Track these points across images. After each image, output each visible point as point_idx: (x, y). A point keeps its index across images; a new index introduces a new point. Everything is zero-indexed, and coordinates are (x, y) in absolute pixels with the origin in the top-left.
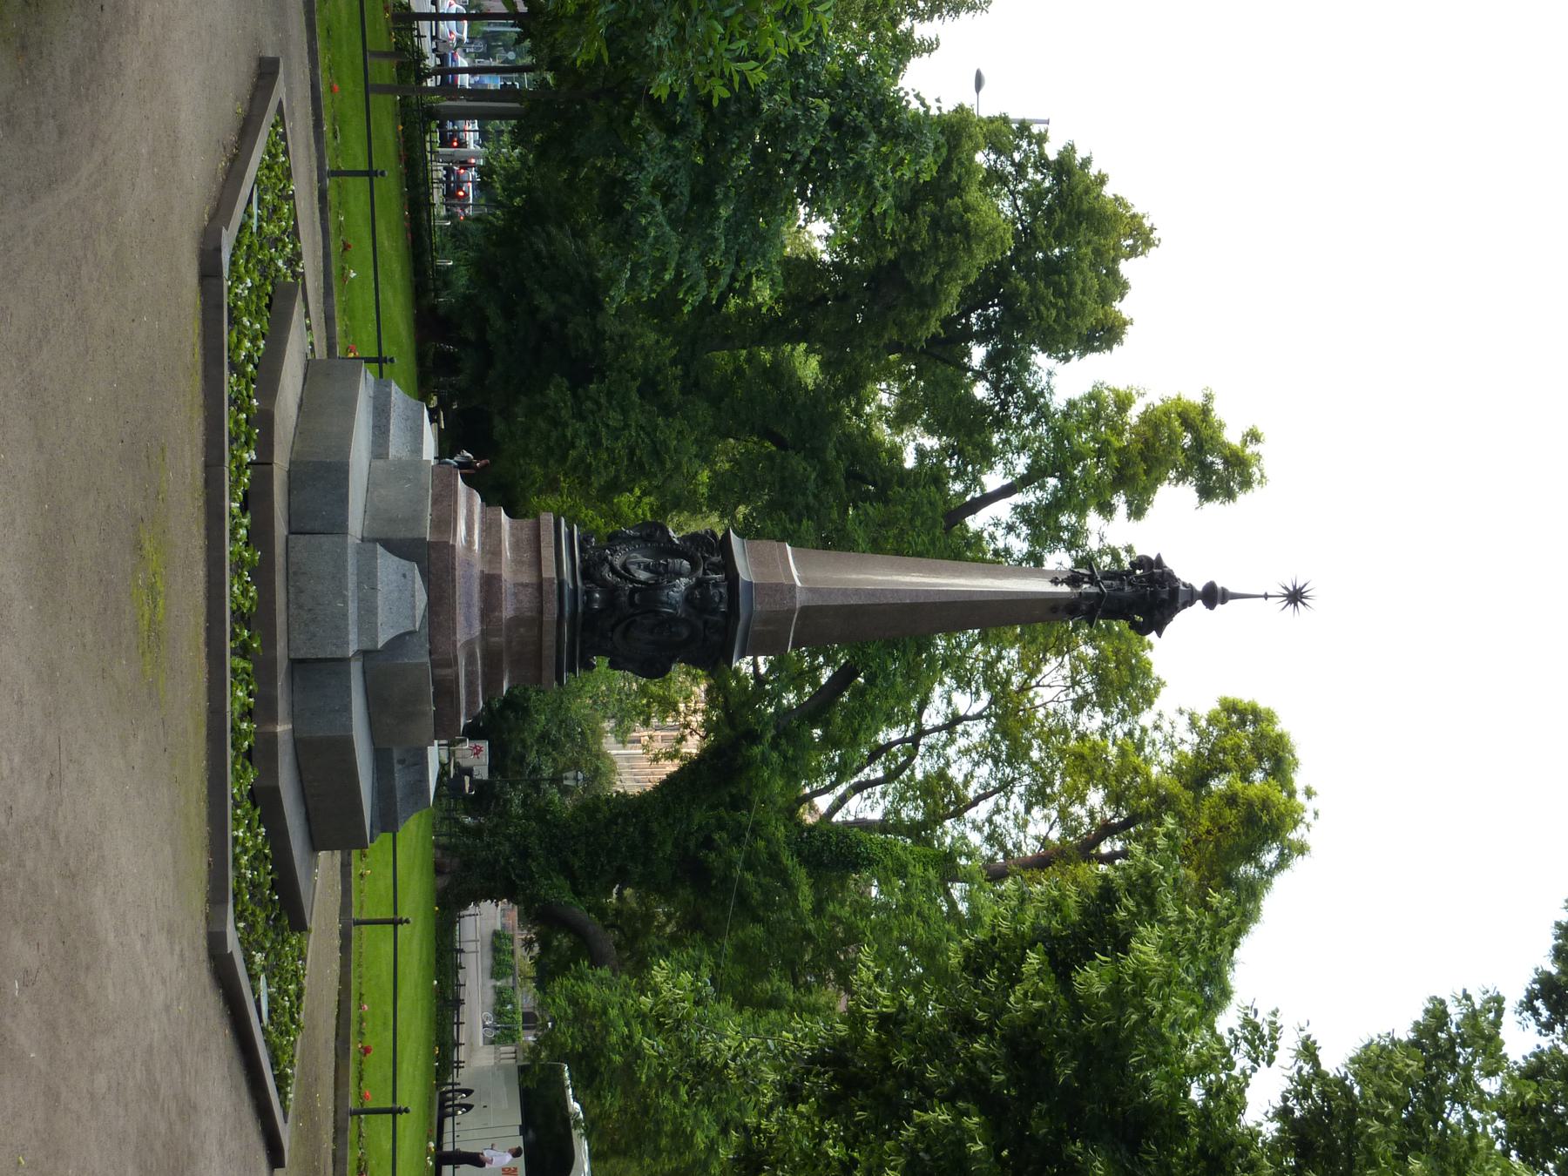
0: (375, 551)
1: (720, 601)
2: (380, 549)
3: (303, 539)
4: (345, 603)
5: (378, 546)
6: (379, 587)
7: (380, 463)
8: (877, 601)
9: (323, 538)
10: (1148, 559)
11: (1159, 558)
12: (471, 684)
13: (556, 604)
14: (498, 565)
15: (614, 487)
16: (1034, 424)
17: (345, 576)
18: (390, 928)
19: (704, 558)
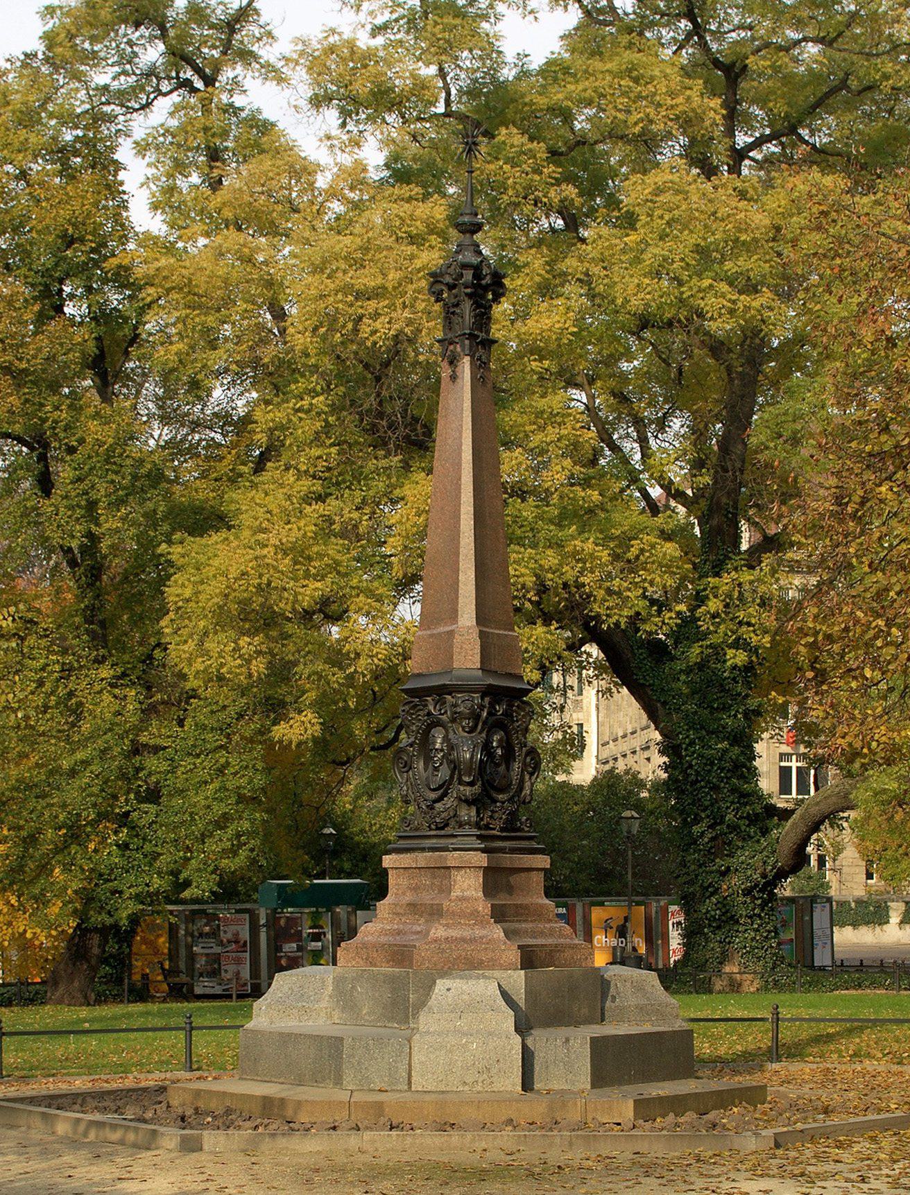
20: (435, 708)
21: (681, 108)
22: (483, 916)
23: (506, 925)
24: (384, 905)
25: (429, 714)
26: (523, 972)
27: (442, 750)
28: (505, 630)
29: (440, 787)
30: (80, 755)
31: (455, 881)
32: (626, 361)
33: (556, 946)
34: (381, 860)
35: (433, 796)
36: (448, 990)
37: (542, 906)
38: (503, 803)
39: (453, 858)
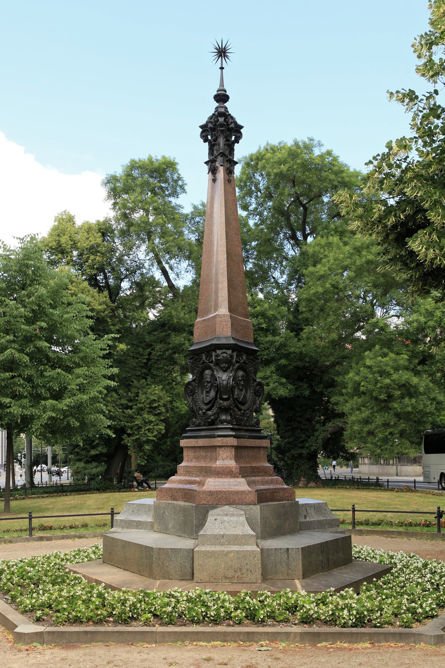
0: (203, 535)
1: (226, 353)
2: (202, 532)
3: (196, 574)
4: (231, 552)
5: (200, 533)
6: (222, 533)
7: (156, 526)
8: (226, 272)
9: (196, 563)
10: (202, 132)
11: (201, 127)
12: (267, 483)
13: (228, 439)
14: (208, 468)
15: (130, 608)
16: (158, 470)
17: (216, 552)
18: (356, 513)
19: (203, 363)
20: (206, 359)
21: (405, 349)
22: (235, 474)
23: (248, 479)
24: (181, 466)
25: (204, 362)
26: (258, 507)
27: (210, 382)
28: (244, 318)
29: (210, 402)
30: (12, 381)
31: (219, 453)
32: (25, 485)
33: (275, 489)
34: (179, 442)
35: (206, 407)
36: (216, 520)
37: (266, 467)
38: (245, 411)
39: (218, 441)
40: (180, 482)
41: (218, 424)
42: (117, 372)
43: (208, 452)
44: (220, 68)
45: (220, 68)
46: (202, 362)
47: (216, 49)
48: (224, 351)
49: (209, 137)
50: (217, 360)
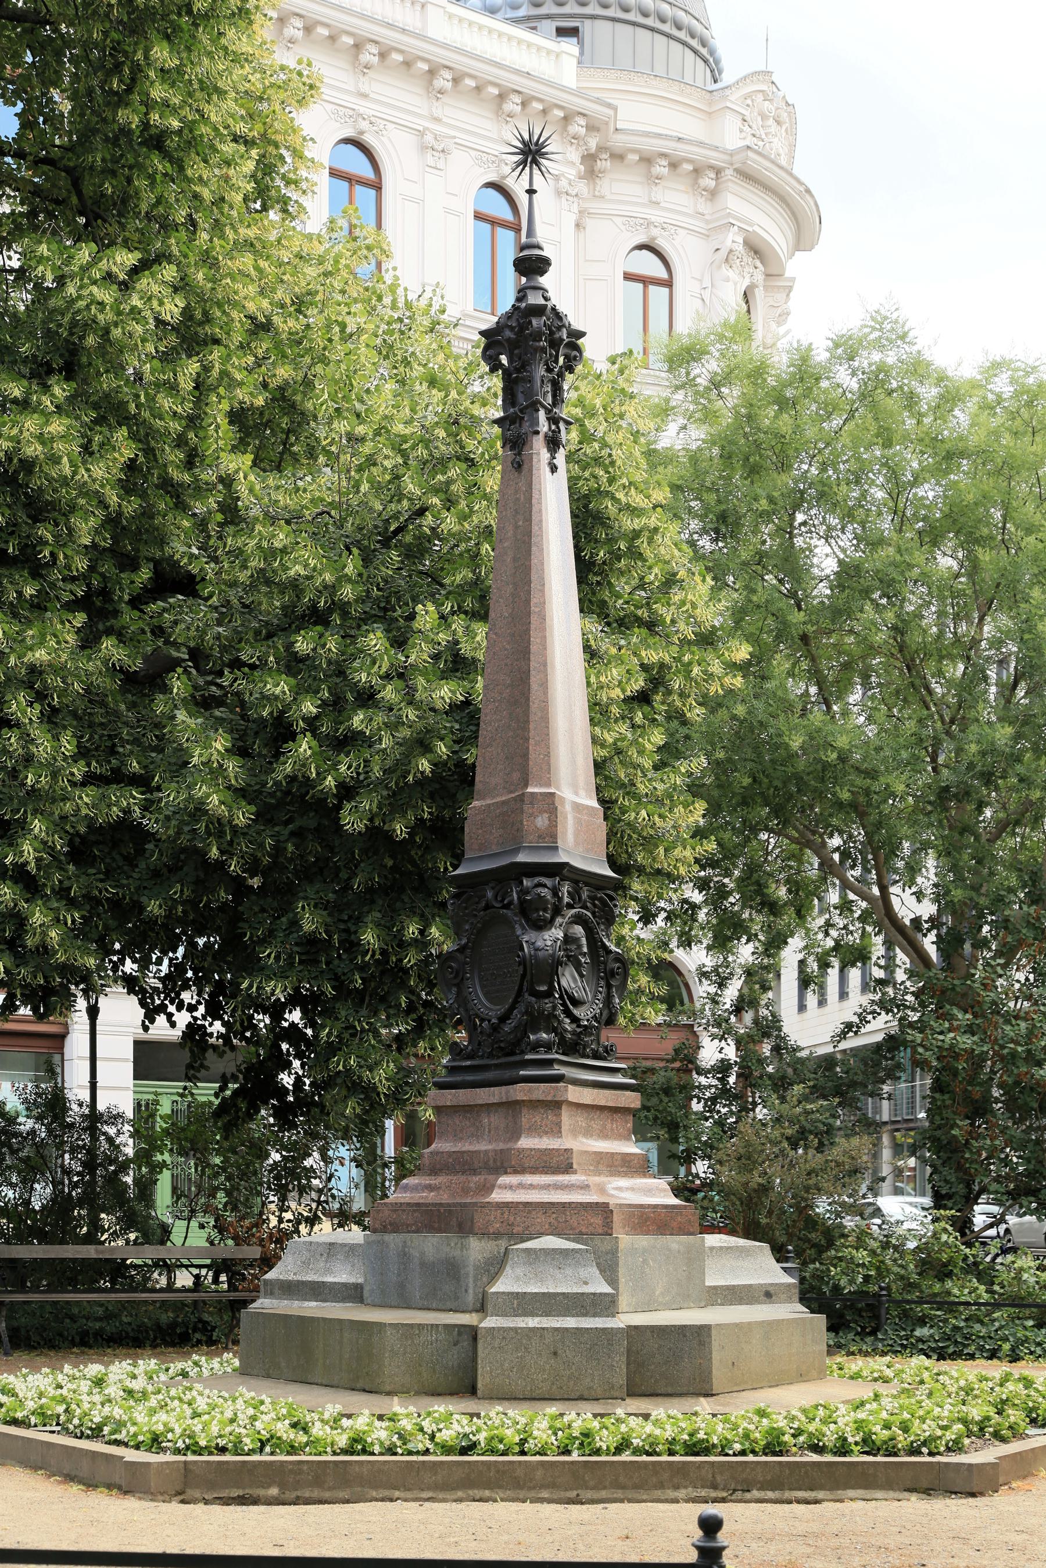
19: (488, 907)
25: (488, 907)
40: (415, 1188)
41: (523, 1052)
42: (818, 359)
43: (593, 1119)
44: (528, 191)
45: (528, 191)
46: (483, 904)
47: (523, 142)
48: (537, 880)
49: (504, 359)
50: (522, 902)
